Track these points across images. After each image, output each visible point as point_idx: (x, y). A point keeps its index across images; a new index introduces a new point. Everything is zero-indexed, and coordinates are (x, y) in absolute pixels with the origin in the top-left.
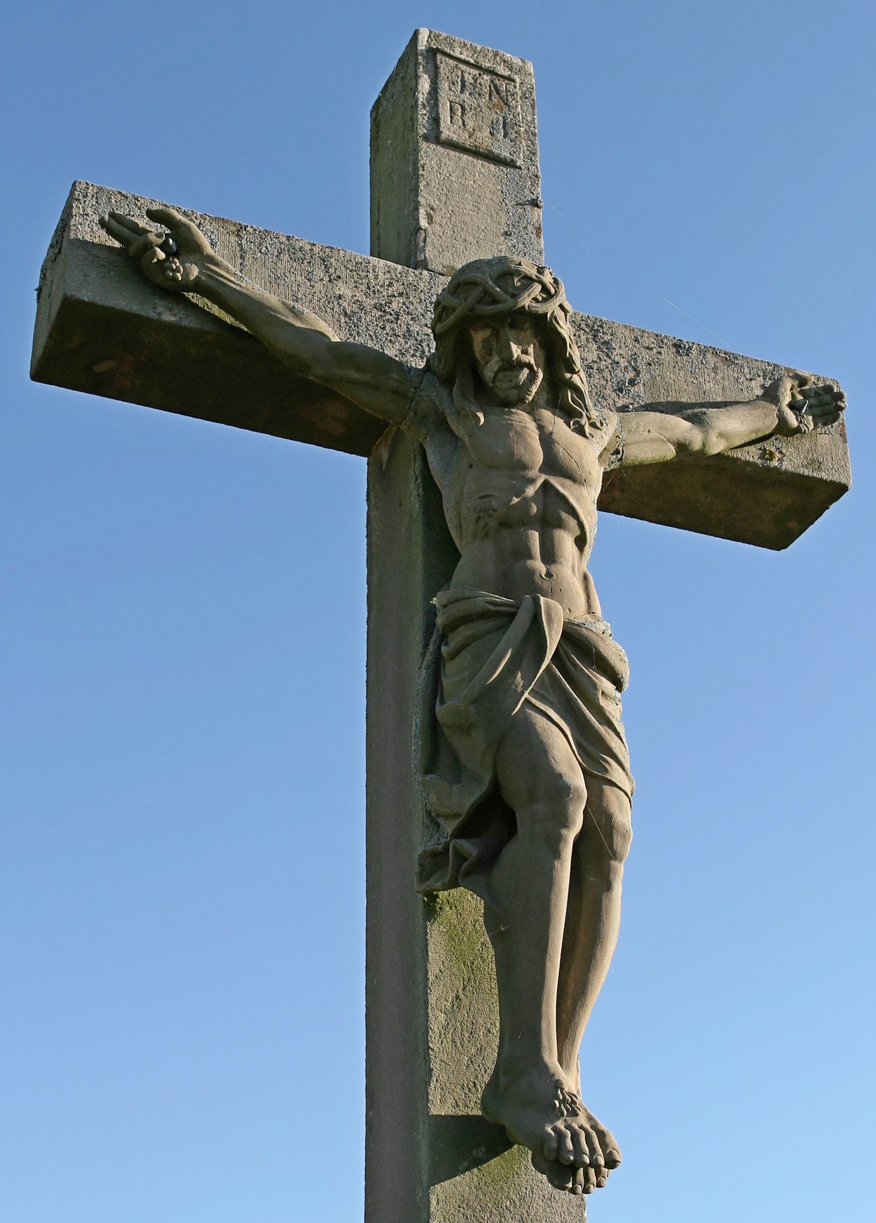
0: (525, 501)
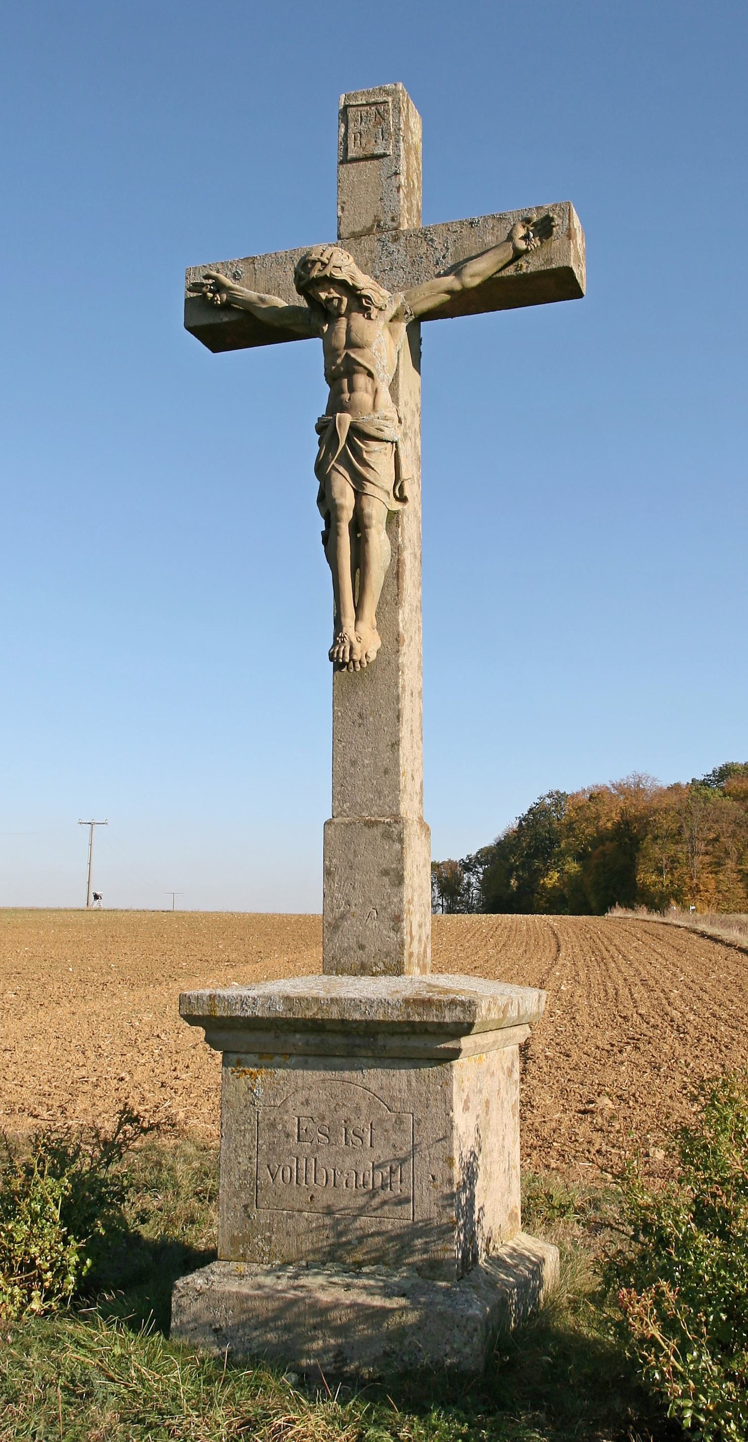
0: (338, 366)
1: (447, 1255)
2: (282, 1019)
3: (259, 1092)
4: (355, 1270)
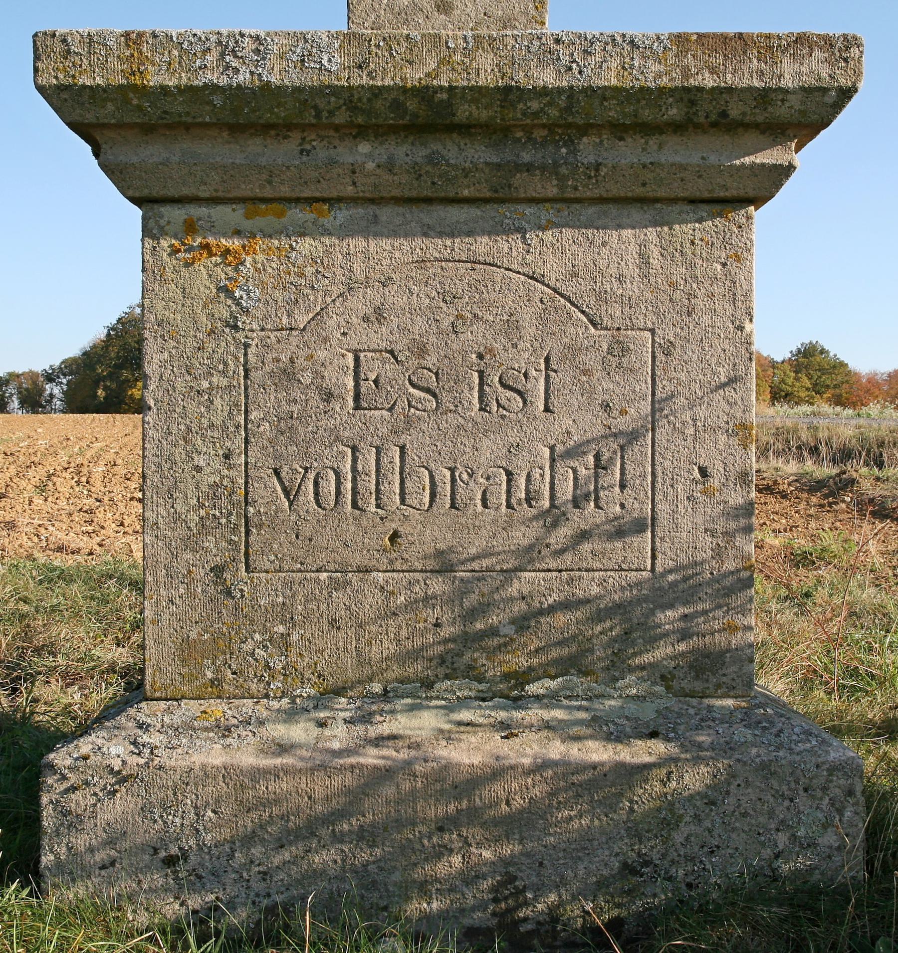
1: (737, 640)
2: (336, 91)
3: (250, 295)
4: (513, 690)
